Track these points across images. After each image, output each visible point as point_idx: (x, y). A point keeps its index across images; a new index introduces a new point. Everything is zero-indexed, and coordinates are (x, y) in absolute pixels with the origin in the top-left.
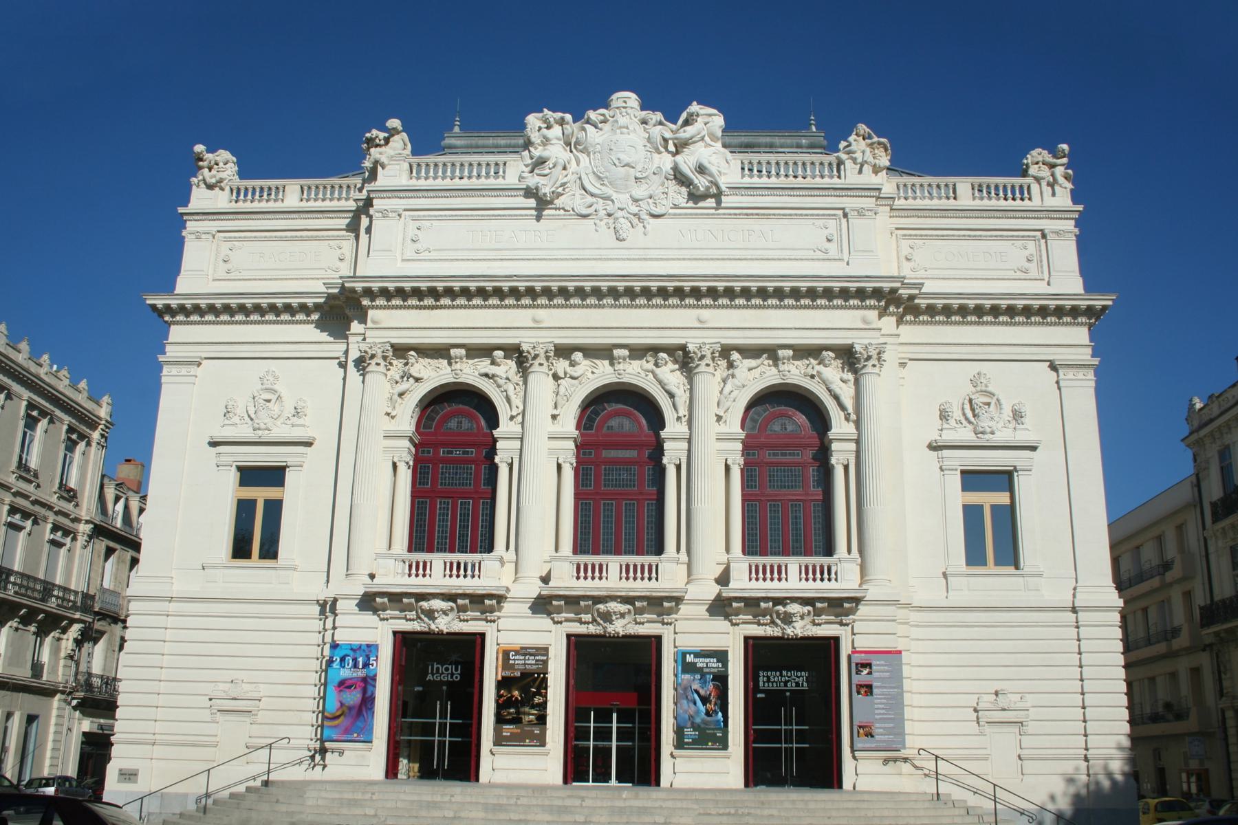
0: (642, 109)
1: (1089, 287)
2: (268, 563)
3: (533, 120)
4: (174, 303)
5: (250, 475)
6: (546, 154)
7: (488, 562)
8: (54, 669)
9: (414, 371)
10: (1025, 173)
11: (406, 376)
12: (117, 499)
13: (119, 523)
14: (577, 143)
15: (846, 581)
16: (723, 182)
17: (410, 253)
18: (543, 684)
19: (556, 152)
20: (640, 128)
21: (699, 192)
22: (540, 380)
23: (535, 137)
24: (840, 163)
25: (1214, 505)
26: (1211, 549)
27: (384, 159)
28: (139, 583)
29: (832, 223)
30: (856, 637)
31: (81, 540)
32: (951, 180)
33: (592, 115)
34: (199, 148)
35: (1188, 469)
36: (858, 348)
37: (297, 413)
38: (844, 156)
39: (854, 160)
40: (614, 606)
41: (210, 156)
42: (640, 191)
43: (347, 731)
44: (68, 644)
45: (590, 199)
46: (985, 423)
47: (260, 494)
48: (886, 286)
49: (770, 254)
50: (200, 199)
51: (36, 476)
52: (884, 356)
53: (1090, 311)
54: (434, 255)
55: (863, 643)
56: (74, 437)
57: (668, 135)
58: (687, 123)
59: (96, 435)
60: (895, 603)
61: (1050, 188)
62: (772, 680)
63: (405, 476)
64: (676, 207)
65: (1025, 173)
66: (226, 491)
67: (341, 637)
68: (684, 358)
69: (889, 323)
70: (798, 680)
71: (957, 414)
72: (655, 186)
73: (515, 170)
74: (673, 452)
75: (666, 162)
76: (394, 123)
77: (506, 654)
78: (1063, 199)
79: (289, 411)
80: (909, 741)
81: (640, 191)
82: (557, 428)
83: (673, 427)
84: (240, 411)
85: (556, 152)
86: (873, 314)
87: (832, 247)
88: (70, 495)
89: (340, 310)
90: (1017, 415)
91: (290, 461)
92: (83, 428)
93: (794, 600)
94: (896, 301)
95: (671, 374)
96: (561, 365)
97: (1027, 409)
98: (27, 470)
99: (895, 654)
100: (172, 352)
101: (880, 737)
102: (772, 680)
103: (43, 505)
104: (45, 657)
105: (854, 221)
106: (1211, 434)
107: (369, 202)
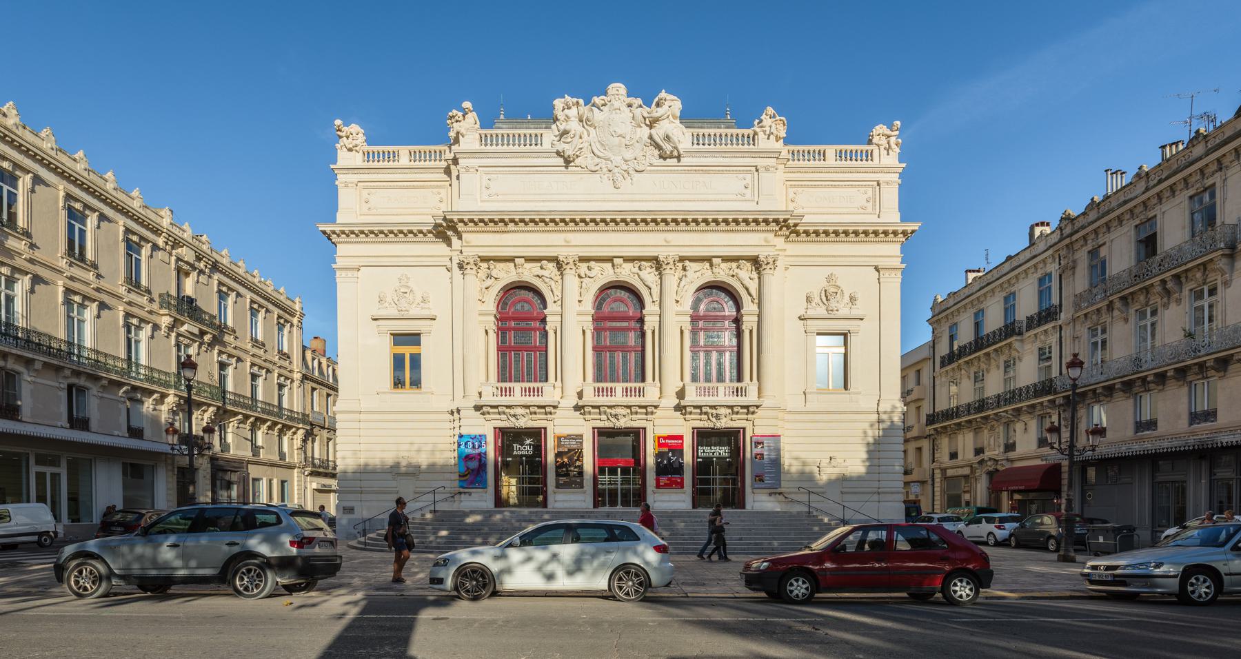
0: (628, 96)
1: (904, 219)
2: (415, 390)
3: (558, 103)
4: (337, 229)
5: (401, 338)
6: (568, 128)
7: (547, 387)
8: (292, 456)
9: (494, 273)
10: (870, 142)
11: (489, 276)
12: (313, 359)
13: (316, 373)
14: (588, 119)
15: (751, 397)
16: (681, 147)
17: (485, 197)
18: (580, 455)
19: (574, 126)
20: (627, 110)
21: (666, 152)
22: (571, 280)
23: (560, 115)
24: (755, 134)
25: (943, 358)
26: (937, 382)
27: (462, 131)
28: (343, 403)
29: (748, 176)
30: (757, 427)
31: (296, 384)
32: (822, 147)
33: (596, 100)
34: (338, 122)
35: (928, 337)
36: (762, 258)
37: (424, 301)
38: (758, 130)
39: (764, 132)
40: (620, 411)
41: (345, 129)
42: (629, 155)
43: (472, 482)
44: (297, 442)
45: (597, 160)
46: (833, 304)
47: (407, 351)
48: (781, 217)
49: (710, 197)
50: (345, 159)
51: (264, 345)
52: (778, 263)
53: (904, 233)
54: (500, 198)
55: (758, 431)
56: (282, 321)
57: (646, 115)
58: (658, 105)
59: (295, 321)
60: (779, 409)
61: (886, 153)
62: (706, 452)
63: (493, 337)
64: (651, 165)
65: (870, 142)
66: (384, 351)
67: (464, 431)
68: (657, 263)
69: (779, 242)
70: (722, 451)
71: (817, 299)
72: (637, 151)
73: (549, 137)
74: (651, 322)
75: (645, 131)
76: (467, 105)
77: (559, 438)
78: (892, 160)
79: (419, 299)
80: (783, 484)
81: (629, 155)
82: (581, 308)
83: (650, 308)
84: (389, 299)
85: (574, 126)
86: (771, 235)
87: (748, 192)
88: (286, 356)
89: (445, 230)
90: (853, 299)
91: (423, 330)
92: (287, 316)
93: (197, 585)
94: (787, 226)
95: (649, 275)
96: (583, 267)
97: (859, 296)
98: (256, 341)
99: (776, 437)
100: (340, 262)
101: (767, 481)
102: (706, 452)
103: (270, 362)
104: (286, 449)
105: (763, 174)
106: (947, 316)
107: (455, 161)
